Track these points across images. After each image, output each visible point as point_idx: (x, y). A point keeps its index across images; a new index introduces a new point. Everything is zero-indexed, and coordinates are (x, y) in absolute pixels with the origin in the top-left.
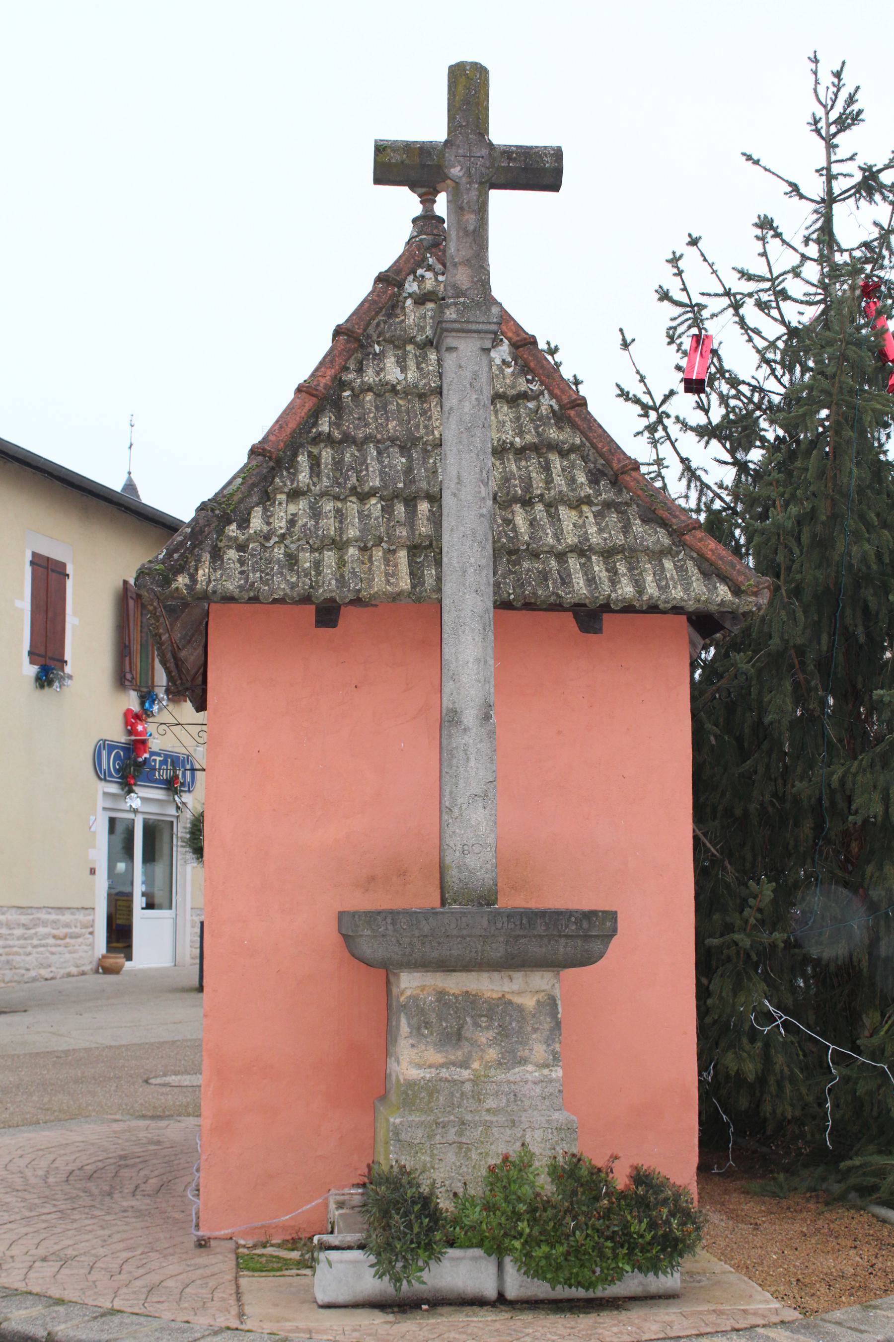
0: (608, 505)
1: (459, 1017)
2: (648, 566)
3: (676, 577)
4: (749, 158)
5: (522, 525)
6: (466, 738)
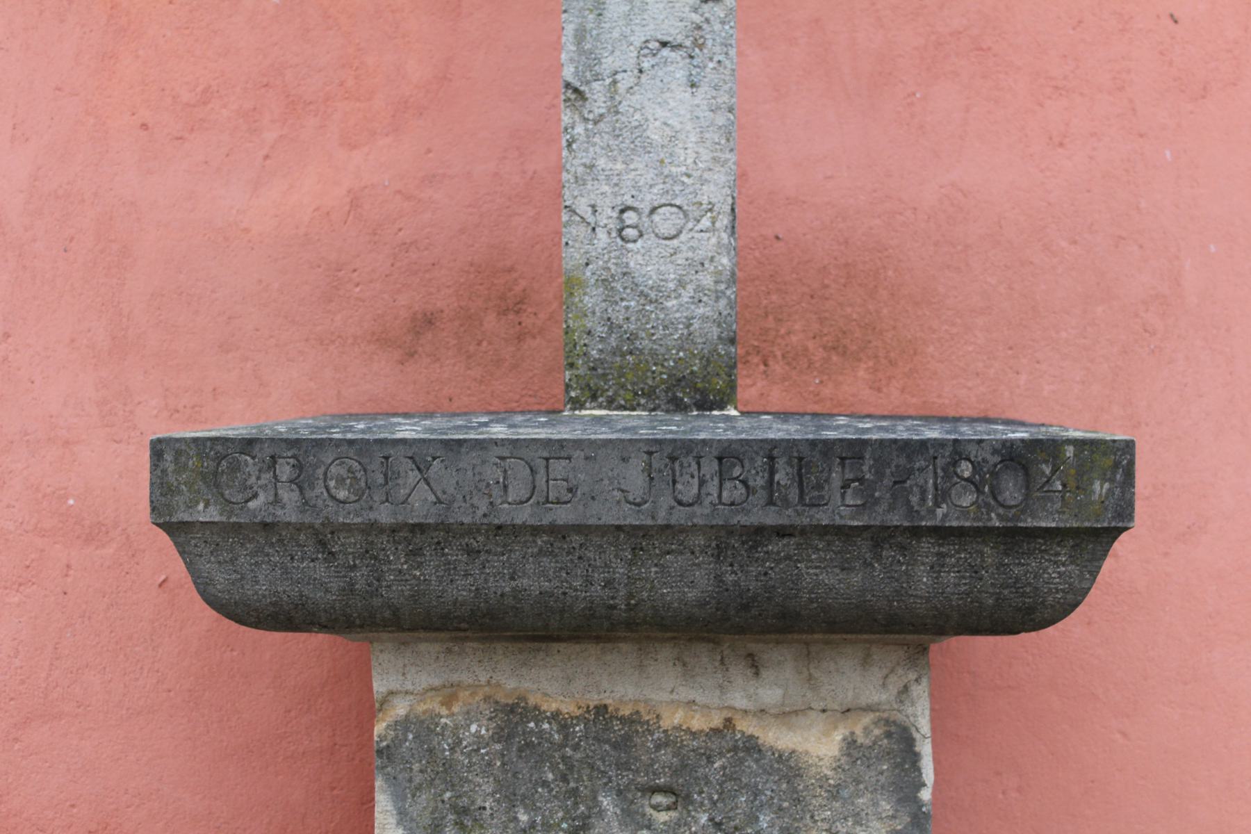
1: (574, 793)
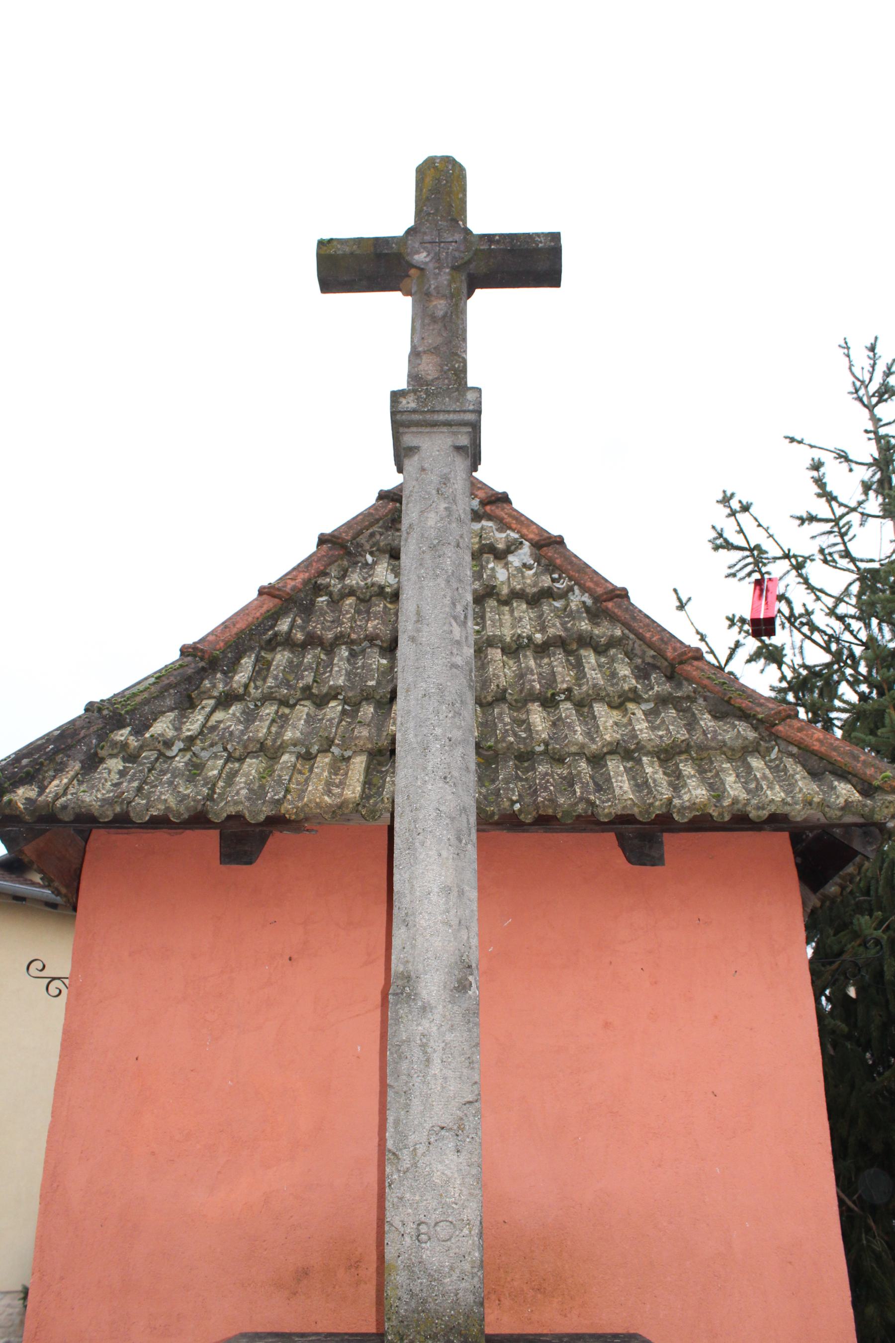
0: (663, 701)
2: (726, 765)
3: (770, 776)
4: (792, 440)
5: (539, 723)
6: (425, 1023)
